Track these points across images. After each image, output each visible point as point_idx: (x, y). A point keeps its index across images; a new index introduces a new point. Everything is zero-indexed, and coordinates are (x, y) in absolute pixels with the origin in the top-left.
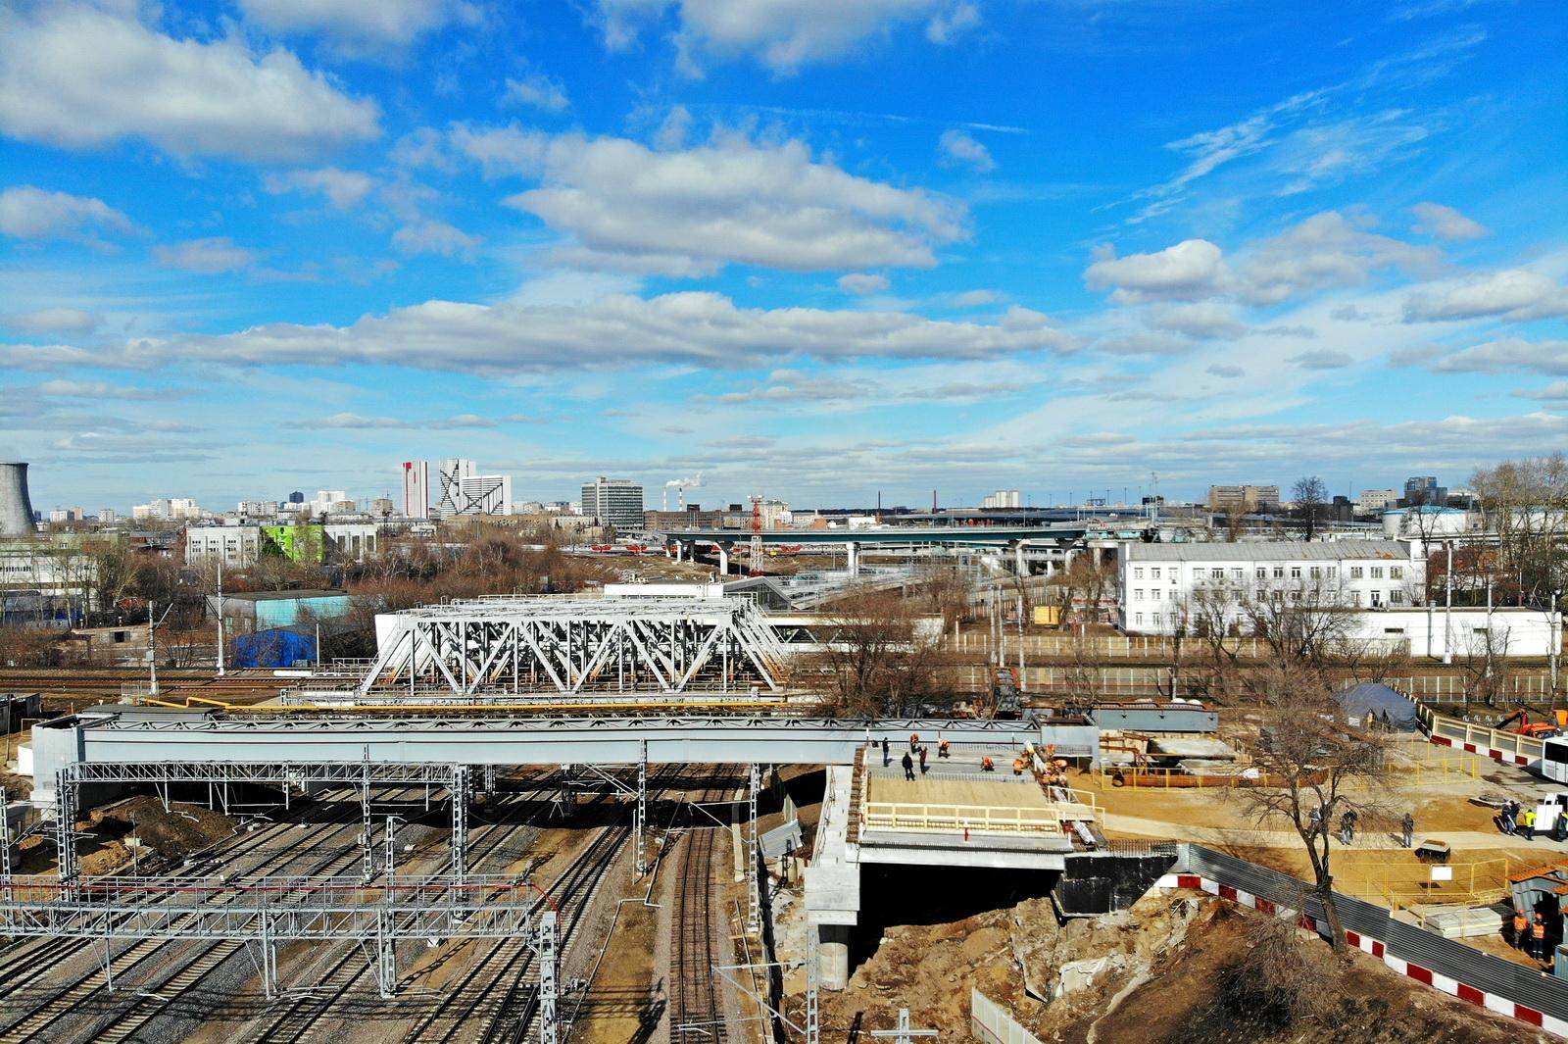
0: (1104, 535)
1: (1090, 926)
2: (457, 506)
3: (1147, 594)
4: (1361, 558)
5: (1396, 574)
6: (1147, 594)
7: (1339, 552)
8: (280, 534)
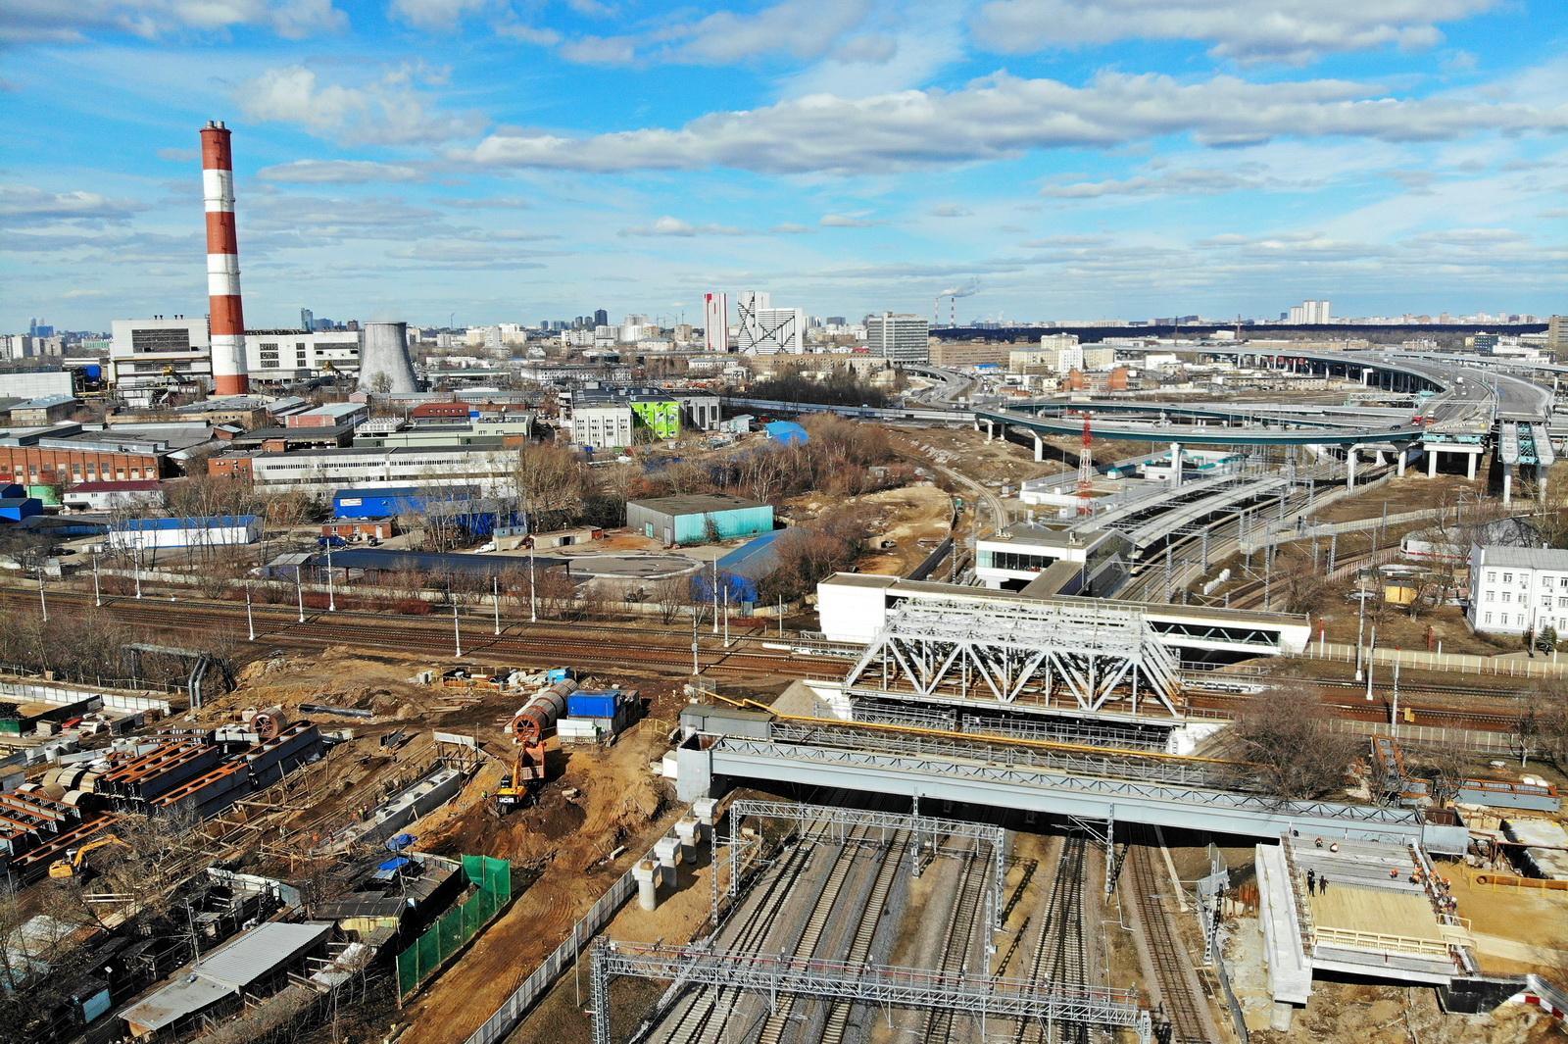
0: (1443, 438)
1: (1463, 1021)
3: (1498, 596)
6: (1498, 596)
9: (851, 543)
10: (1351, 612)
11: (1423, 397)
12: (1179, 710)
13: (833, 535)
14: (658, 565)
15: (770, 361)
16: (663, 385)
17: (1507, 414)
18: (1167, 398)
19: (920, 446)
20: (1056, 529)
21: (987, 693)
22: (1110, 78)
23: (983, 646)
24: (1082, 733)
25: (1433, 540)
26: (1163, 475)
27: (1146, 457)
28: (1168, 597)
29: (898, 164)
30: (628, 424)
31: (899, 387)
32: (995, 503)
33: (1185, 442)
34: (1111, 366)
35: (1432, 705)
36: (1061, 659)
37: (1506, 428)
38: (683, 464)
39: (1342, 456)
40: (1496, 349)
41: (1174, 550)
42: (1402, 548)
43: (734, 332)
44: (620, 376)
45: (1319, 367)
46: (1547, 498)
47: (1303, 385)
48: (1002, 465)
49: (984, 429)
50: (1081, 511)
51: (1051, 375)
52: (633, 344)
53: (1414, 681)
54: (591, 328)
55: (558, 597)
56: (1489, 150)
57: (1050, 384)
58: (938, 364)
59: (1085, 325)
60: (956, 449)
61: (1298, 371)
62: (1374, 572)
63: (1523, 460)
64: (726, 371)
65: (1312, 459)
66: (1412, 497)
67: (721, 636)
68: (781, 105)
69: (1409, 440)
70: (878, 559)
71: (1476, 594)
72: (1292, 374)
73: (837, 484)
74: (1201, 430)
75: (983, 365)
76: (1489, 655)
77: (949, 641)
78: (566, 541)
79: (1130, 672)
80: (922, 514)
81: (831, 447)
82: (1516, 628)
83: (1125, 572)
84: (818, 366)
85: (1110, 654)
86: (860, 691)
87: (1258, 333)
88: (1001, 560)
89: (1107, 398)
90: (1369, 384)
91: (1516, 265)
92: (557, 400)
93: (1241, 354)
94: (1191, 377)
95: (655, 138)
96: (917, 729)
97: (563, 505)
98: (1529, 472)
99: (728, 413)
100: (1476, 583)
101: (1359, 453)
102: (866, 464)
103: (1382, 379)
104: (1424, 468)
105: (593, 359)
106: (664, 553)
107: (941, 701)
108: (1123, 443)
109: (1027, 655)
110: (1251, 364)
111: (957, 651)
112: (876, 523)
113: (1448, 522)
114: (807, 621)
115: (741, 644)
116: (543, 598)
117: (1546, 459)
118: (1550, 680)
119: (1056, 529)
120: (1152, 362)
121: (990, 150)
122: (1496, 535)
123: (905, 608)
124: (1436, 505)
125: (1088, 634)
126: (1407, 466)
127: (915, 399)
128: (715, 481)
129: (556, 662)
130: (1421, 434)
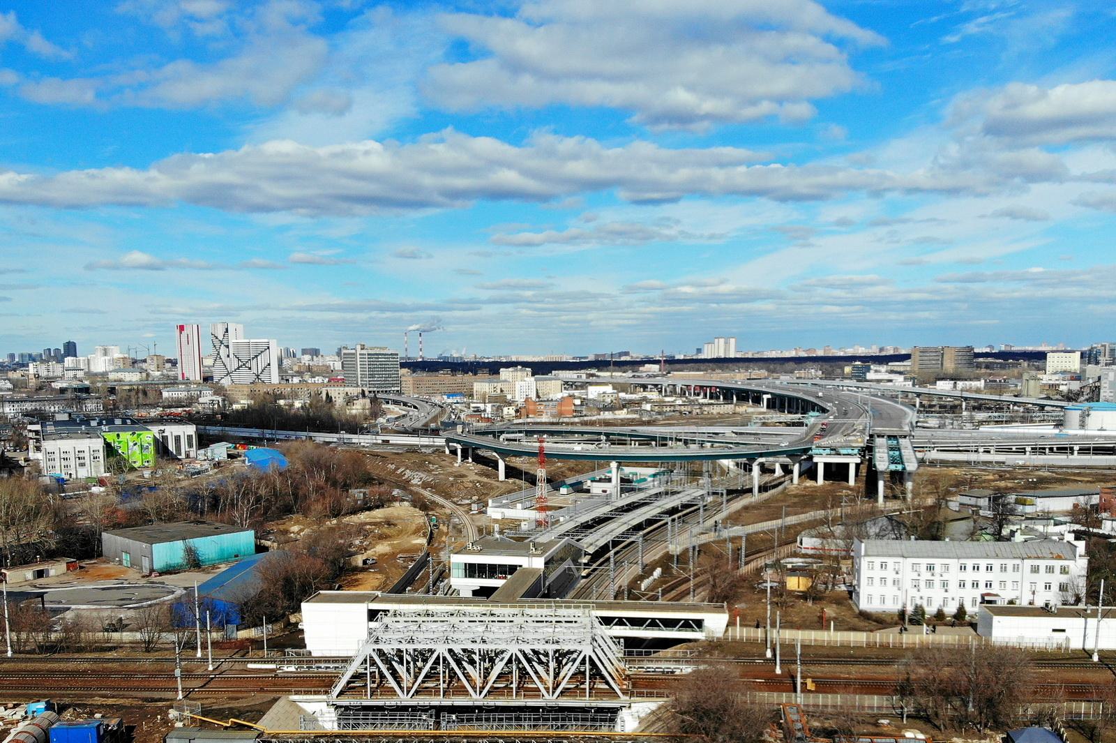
0: (828, 451)
2: (228, 367)
3: (877, 581)
4: (1038, 558)
5: (1064, 571)
6: (877, 581)
7: (1023, 552)
8: (116, 439)
9: (334, 562)
10: (760, 600)
11: (812, 418)
12: (625, 692)
13: (315, 556)
14: (137, 594)
15: (246, 391)
16: (136, 413)
17: (879, 429)
18: (607, 423)
19: (397, 469)
20: (519, 540)
21: (462, 691)
22: (544, 138)
23: (457, 649)
24: (545, 720)
25: (823, 536)
26: (605, 489)
27: (591, 474)
28: (612, 594)
29: (359, 208)
30: (101, 455)
31: (375, 413)
32: (466, 519)
33: (622, 461)
34: (559, 396)
35: (829, 675)
36: (525, 655)
37: (879, 441)
38: (160, 493)
39: (748, 469)
40: (870, 376)
41: (616, 553)
42: (798, 544)
43: (208, 362)
44: (90, 406)
45: (727, 394)
46: (913, 499)
47: (715, 410)
48: (471, 485)
49: (454, 452)
50: (539, 523)
51: (509, 404)
52: (104, 374)
53: (814, 655)
54: (60, 360)
55: (34, 630)
56: (855, 210)
57: (509, 411)
58: (410, 394)
59: (536, 359)
60: (430, 471)
61: (711, 398)
62: (777, 565)
63: (893, 467)
64: (201, 400)
65: (724, 472)
66: (806, 501)
67: (204, 659)
68: (245, 149)
69: (801, 454)
70: (360, 576)
71: (859, 581)
72: (707, 401)
73: (319, 507)
74: (634, 450)
75: (450, 395)
76: (871, 631)
77: (427, 647)
78: (40, 574)
79: (583, 662)
80: (400, 532)
81: (311, 473)
82: (892, 607)
83: (577, 575)
84: (295, 395)
85: (566, 648)
86: (345, 701)
87: (678, 366)
88: (473, 570)
89: (557, 424)
90: (768, 407)
91: (882, 305)
92: (25, 433)
93: (665, 384)
94: (625, 405)
95: (121, 176)
96: (400, 731)
97: (34, 538)
98: (897, 477)
99: (204, 441)
100: (859, 571)
101: (762, 465)
102: (346, 487)
103: (779, 403)
104: (813, 477)
105: (63, 391)
106: (143, 582)
107: (421, 703)
108: (572, 463)
109: (497, 655)
110: (673, 392)
111: (435, 656)
112: (357, 542)
113: (835, 521)
114: (293, 639)
115: (225, 666)
116: (19, 632)
117: (911, 466)
118: (921, 649)
119: (519, 540)
120: (593, 392)
121: (441, 199)
122: (873, 530)
123: (387, 620)
124: (824, 508)
125: (547, 631)
126: (800, 475)
127: (390, 426)
128: (193, 508)
129: (36, 695)
130: (810, 449)
